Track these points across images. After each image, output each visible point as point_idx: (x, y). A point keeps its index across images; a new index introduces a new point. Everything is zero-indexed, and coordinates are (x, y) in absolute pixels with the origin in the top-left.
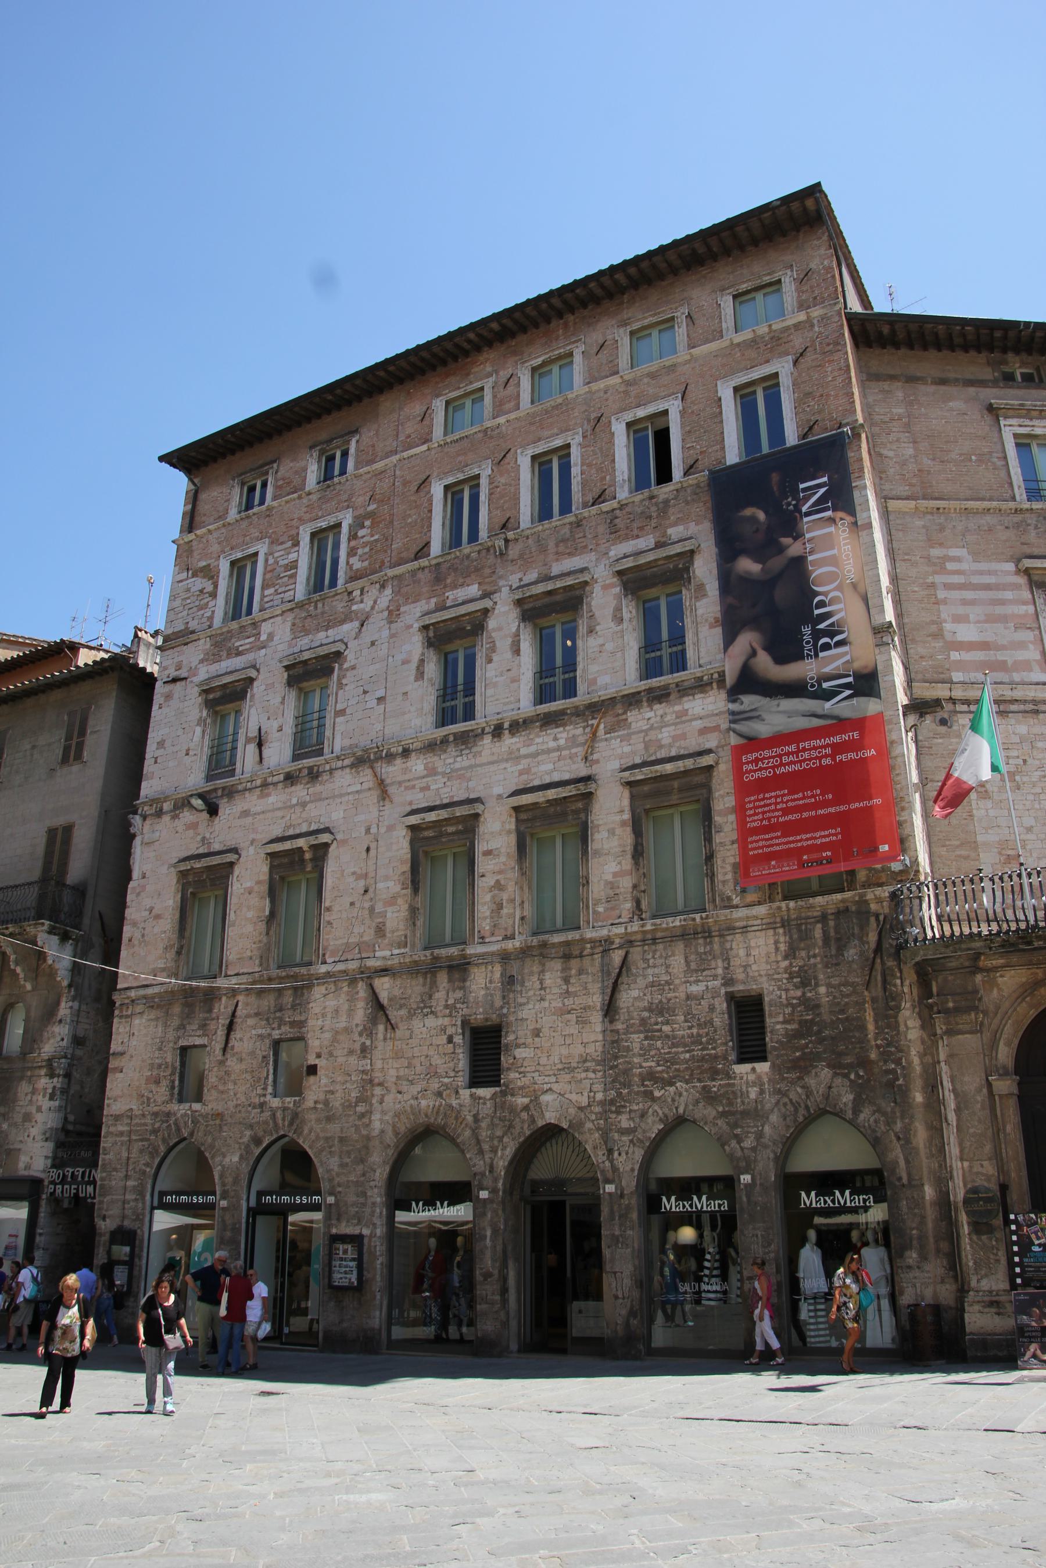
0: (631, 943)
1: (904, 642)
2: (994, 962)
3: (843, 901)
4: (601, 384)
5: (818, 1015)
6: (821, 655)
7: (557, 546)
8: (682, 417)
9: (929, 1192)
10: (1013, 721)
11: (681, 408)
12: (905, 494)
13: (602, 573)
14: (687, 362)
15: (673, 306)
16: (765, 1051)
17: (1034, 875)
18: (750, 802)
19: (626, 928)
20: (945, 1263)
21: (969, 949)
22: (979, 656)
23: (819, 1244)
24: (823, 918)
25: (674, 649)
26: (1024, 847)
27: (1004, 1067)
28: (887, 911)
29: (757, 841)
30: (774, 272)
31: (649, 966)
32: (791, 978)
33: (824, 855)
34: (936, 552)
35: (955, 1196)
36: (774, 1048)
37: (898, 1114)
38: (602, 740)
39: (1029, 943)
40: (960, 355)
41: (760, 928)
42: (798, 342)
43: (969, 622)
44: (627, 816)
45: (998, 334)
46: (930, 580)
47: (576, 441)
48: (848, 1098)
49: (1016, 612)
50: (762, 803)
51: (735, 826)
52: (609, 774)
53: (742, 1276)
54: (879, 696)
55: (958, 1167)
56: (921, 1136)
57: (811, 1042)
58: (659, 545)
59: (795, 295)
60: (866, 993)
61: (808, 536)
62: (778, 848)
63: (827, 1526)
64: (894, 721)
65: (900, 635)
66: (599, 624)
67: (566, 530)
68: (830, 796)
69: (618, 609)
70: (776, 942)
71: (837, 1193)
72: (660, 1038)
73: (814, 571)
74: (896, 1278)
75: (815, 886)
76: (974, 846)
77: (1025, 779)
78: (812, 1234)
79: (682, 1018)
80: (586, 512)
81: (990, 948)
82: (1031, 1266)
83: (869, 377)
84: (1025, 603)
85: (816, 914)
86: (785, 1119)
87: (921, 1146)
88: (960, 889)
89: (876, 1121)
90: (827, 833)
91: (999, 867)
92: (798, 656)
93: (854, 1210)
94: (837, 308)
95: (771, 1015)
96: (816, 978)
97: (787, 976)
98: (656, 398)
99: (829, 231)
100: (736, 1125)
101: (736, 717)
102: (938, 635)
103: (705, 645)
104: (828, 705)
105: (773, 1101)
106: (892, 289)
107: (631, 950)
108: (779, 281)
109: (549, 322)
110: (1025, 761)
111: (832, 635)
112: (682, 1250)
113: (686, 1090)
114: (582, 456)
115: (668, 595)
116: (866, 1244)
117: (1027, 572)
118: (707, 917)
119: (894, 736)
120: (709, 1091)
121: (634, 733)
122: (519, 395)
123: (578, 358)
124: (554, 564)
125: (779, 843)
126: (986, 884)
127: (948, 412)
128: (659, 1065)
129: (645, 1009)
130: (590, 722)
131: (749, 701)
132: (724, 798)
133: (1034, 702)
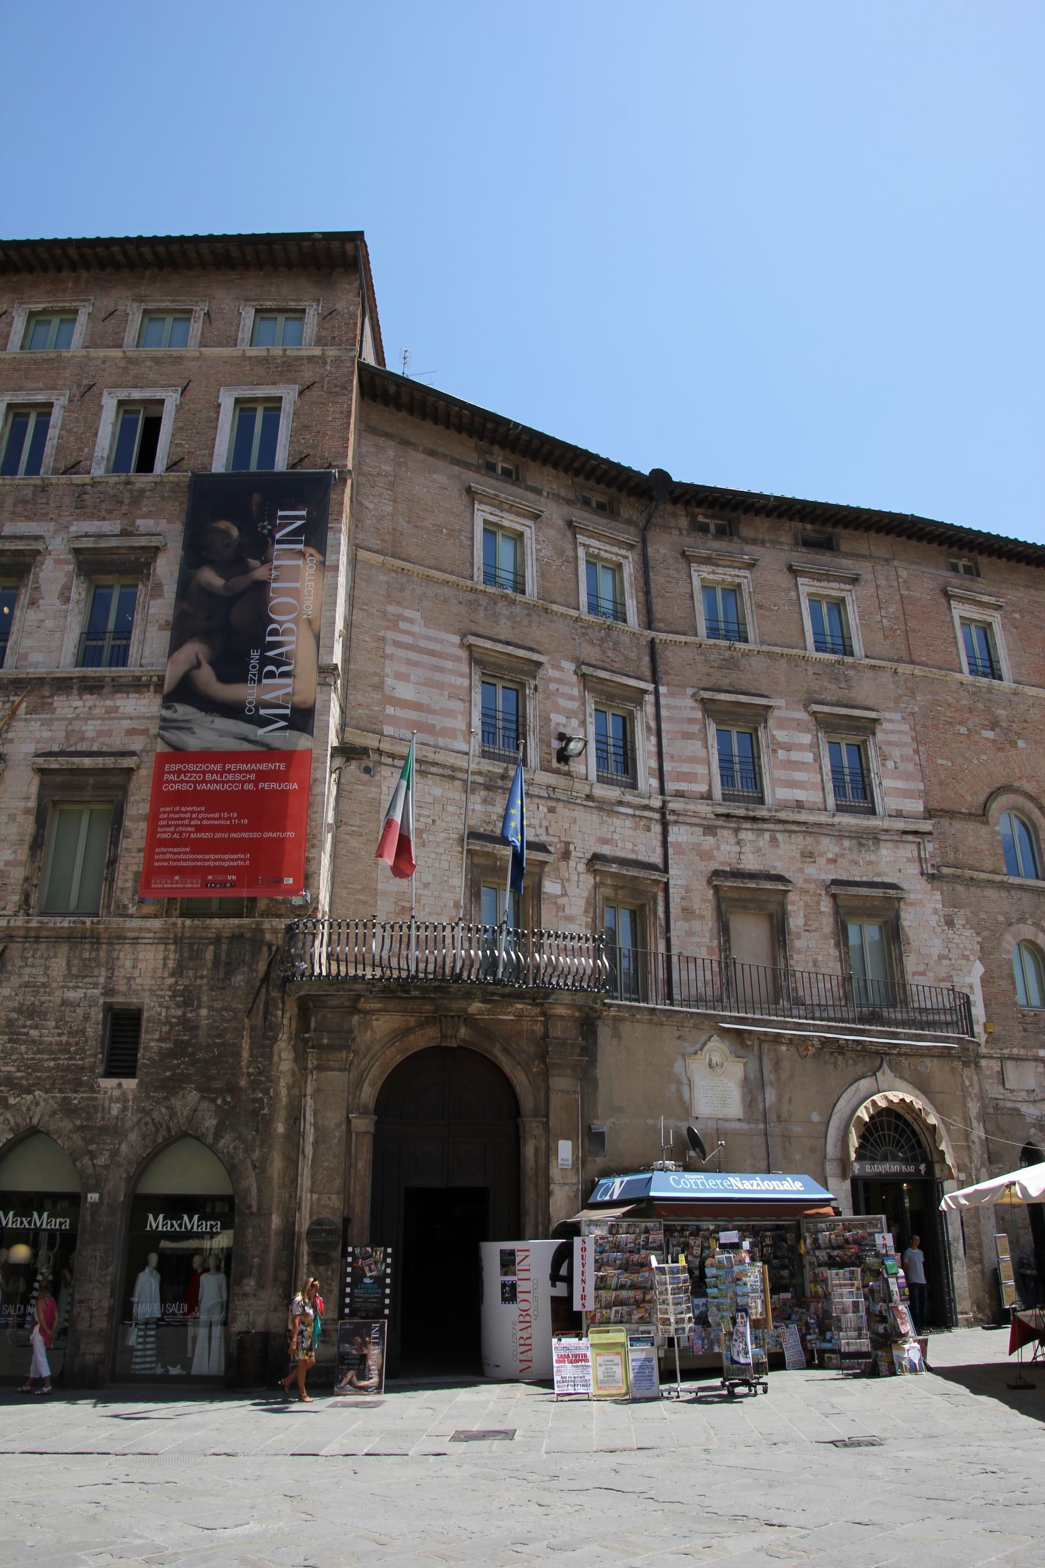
0: (11, 938)
1: (345, 687)
2: (372, 1005)
3: (240, 926)
4: (102, 353)
5: (195, 1036)
6: (264, 681)
7: (15, 505)
8: (177, 411)
9: (276, 1221)
10: (430, 782)
11: (178, 402)
12: (376, 547)
13: (58, 546)
14: (194, 359)
15: (194, 299)
16: (135, 1067)
17: (422, 930)
18: (165, 812)
19: (9, 922)
20: (281, 1291)
21: (351, 990)
22: (412, 715)
23: (160, 1268)
24: (217, 941)
25: (118, 642)
26: (418, 901)
27: (365, 1107)
28: (280, 942)
29: (164, 853)
30: (300, 300)
31: (26, 965)
32: (173, 996)
33: (229, 878)
34: (392, 609)
35: (300, 1228)
36: (145, 1065)
37: (258, 1143)
38: (21, 720)
39: (407, 992)
40: (453, 434)
41: (151, 941)
42: (308, 374)
43: (409, 681)
44: (32, 804)
45: (490, 426)
46: (382, 634)
47: (60, 402)
48: (211, 1122)
49: (453, 682)
50: (177, 816)
51: (145, 834)
52: (21, 758)
53: (73, 1300)
54: (311, 734)
55: (307, 1198)
56: (277, 1165)
57: (183, 1063)
58: (124, 533)
59: (316, 328)
60: (246, 1020)
61: (276, 563)
62: (184, 864)
63: (115, 1560)
64: (321, 760)
65: (343, 679)
66: (42, 598)
67: (28, 492)
68: (246, 821)
69: (67, 588)
70: (166, 958)
71: (186, 1217)
72: (25, 1042)
73: (275, 598)
74: (231, 1306)
75: (215, 907)
76: (374, 893)
77: (431, 838)
78: (153, 1258)
79: (54, 1023)
80: (54, 479)
81: (371, 992)
82: (360, 1297)
83: (367, 429)
84: (462, 676)
85: (210, 935)
86: (144, 1139)
87: (276, 1176)
88: (352, 931)
89: (235, 1148)
90: (236, 857)
91: (393, 916)
92: (241, 678)
93: (200, 1236)
94: (352, 354)
95: (147, 1032)
96: (199, 999)
97: (170, 993)
98: (154, 385)
99: (361, 280)
100: (92, 1141)
101: (166, 724)
102: (379, 687)
103: (150, 646)
104: (261, 732)
105: (135, 1119)
106: (407, 354)
107: (10, 945)
108: (304, 311)
109: (59, 269)
110: (434, 821)
111: (279, 664)
112: (14, 1270)
113: (45, 1100)
114: (64, 420)
115: (123, 586)
116: (206, 1270)
117: (470, 647)
118: (99, 922)
119: (318, 775)
120: (70, 1103)
121: (57, 719)
122: (8, 335)
123: (82, 319)
124: (7, 524)
125: (187, 859)
126: (378, 930)
127: (433, 482)
128: (19, 1071)
129: (14, 1010)
130: (12, 698)
131: (183, 711)
132: (139, 804)
133: (453, 768)
